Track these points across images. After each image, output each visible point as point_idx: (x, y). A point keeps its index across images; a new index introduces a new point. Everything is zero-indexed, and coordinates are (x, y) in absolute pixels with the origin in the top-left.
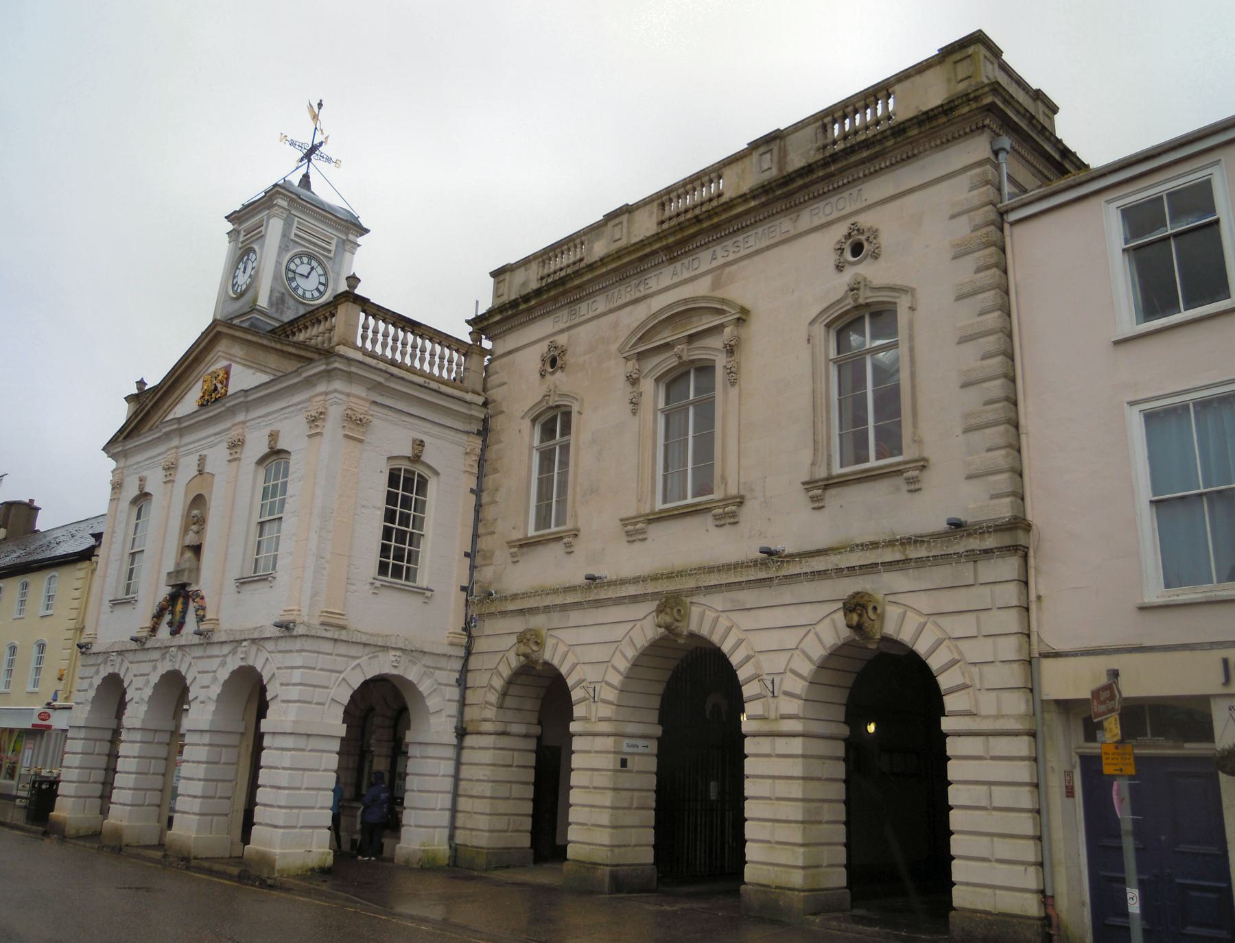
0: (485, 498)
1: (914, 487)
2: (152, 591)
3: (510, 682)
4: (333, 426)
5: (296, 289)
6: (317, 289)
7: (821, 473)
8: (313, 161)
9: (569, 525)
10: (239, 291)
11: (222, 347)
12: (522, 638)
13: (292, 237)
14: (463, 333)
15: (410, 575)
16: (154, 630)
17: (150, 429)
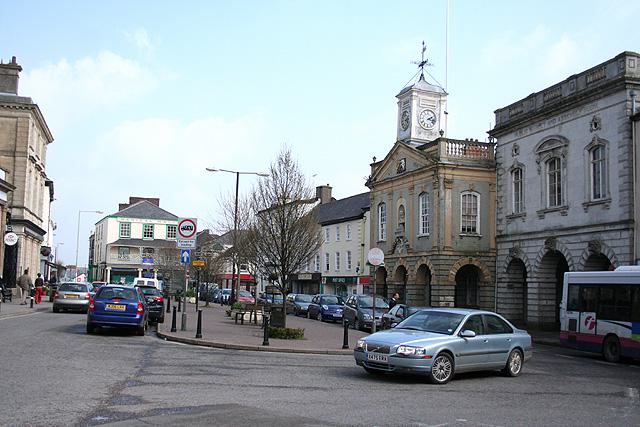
1: (607, 207)
7: (587, 200)
9: (607, 196)
12: (511, 250)
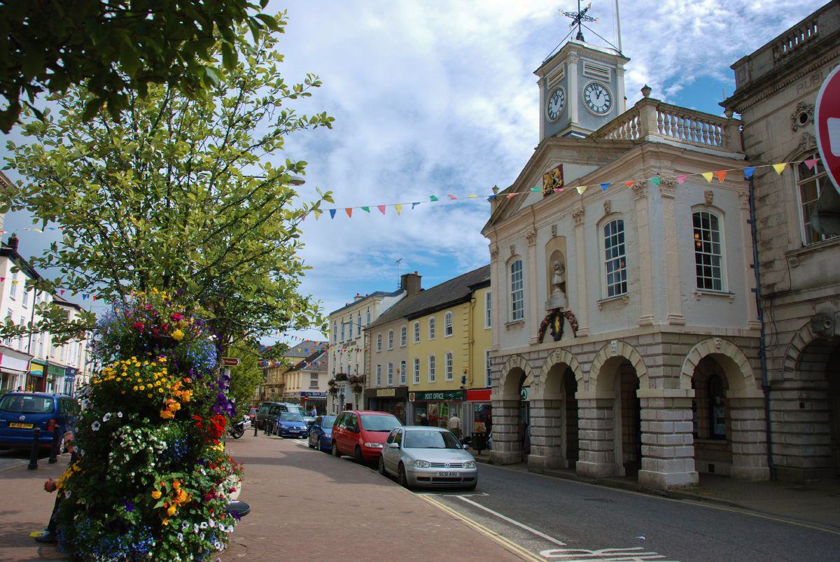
0: (759, 225)
2: (536, 313)
3: (804, 352)
4: (653, 192)
5: (592, 107)
6: (605, 105)
8: (582, 22)
10: (555, 116)
11: (553, 153)
13: (584, 74)
14: (721, 113)
15: (718, 285)
16: (541, 340)
17: (510, 216)
